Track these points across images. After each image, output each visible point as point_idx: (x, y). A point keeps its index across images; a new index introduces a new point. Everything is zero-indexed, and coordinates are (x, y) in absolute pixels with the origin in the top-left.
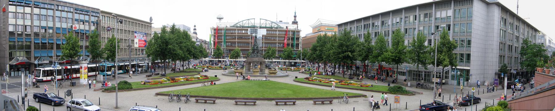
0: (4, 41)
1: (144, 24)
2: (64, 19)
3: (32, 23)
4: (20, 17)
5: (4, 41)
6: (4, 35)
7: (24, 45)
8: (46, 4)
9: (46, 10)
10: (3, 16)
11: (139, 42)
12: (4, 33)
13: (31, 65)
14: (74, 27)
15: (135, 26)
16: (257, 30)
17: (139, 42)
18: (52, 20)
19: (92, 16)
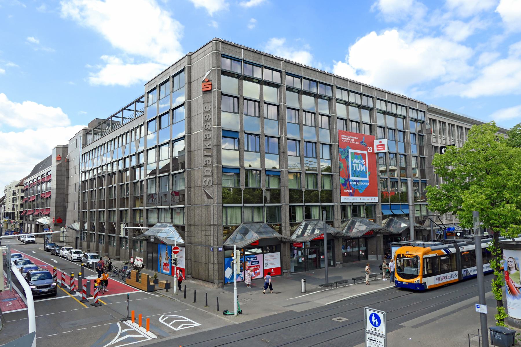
0: (209, 176)
1: (447, 121)
2: (309, 115)
3: (281, 129)
4: (309, 123)
5: (209, 176)
6: (207, 159)
7: (304, 190)
8: (239, 60)
9: (236, 81)
10: (203, 103)
11: (29, 231)
12: (206, 154)
13: (335, 241)
14: (378, 146)
15: (440, 133)
16: (356, 222)
17: (26, 231)
18: (402, 140)
19: (289, 89)
